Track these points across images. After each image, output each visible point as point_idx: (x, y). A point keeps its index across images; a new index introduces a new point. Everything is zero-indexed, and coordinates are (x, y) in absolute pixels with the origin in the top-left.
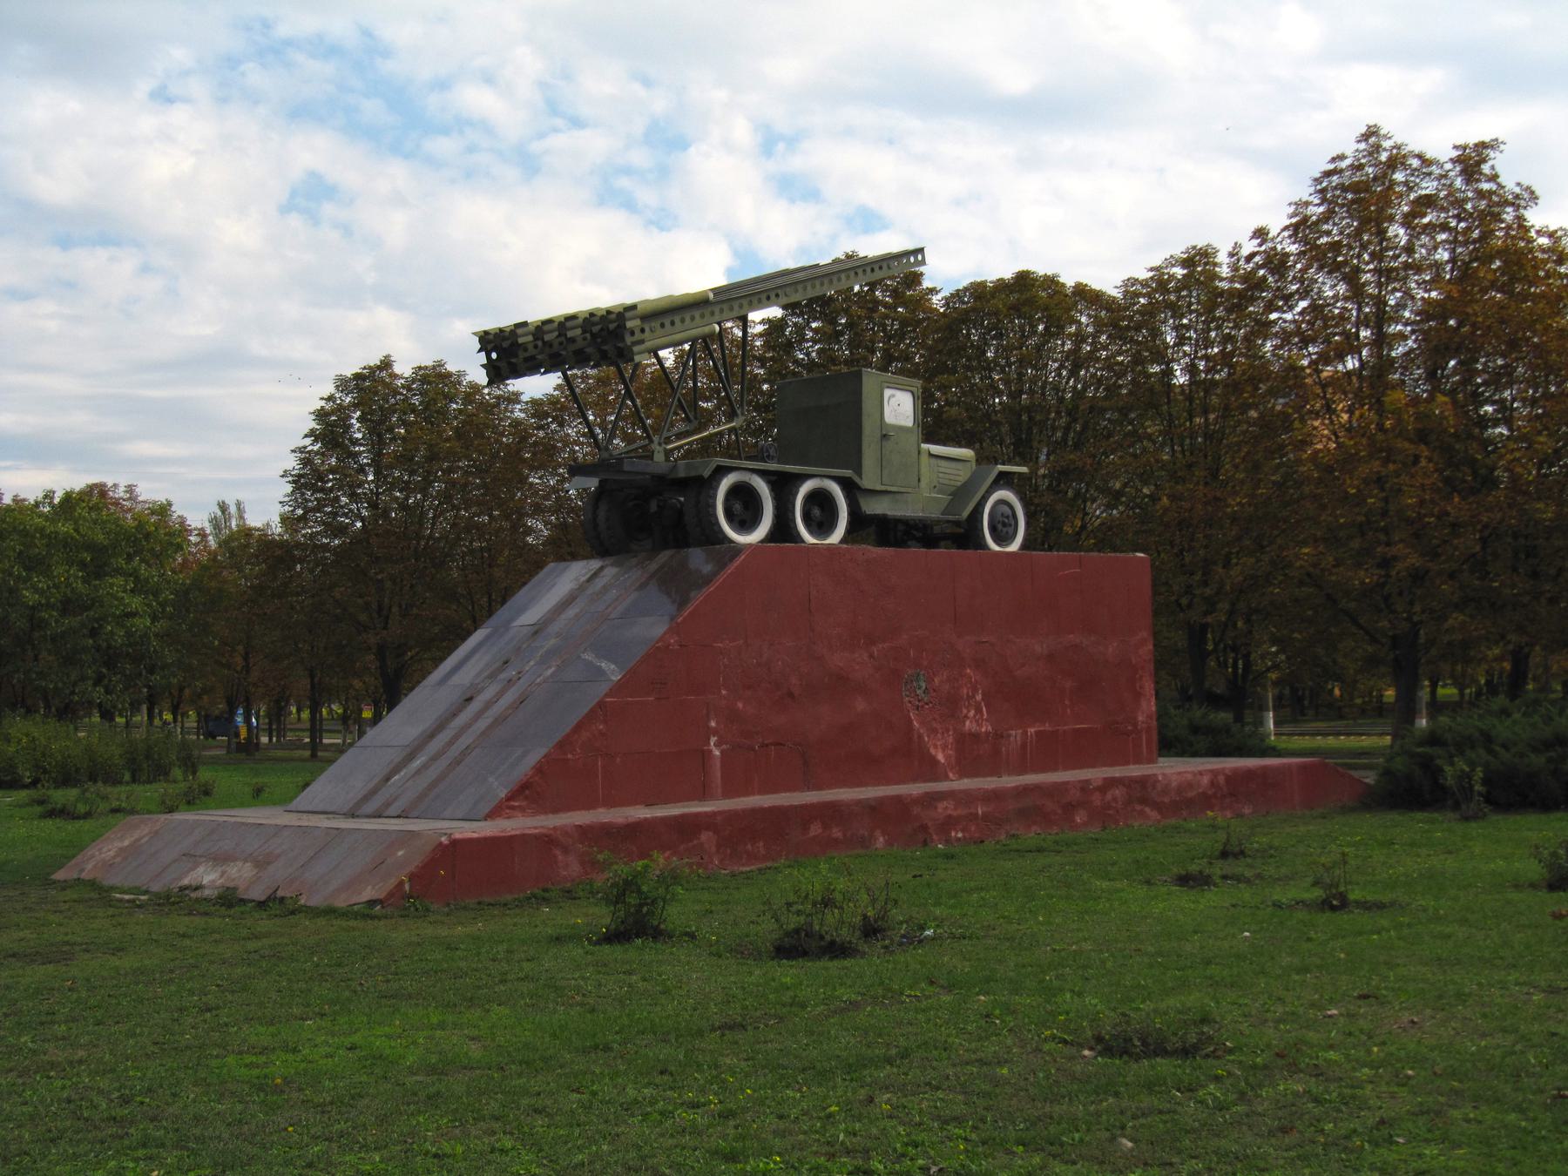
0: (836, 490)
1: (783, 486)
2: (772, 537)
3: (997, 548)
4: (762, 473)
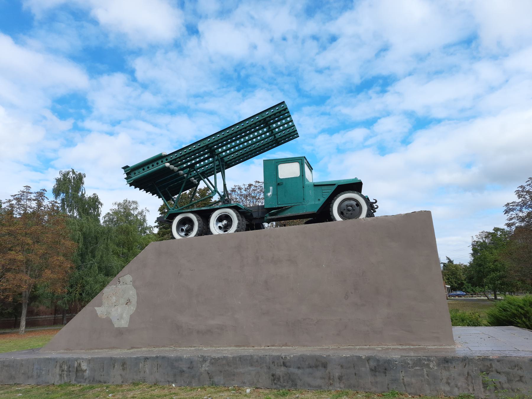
4: (192, 212)
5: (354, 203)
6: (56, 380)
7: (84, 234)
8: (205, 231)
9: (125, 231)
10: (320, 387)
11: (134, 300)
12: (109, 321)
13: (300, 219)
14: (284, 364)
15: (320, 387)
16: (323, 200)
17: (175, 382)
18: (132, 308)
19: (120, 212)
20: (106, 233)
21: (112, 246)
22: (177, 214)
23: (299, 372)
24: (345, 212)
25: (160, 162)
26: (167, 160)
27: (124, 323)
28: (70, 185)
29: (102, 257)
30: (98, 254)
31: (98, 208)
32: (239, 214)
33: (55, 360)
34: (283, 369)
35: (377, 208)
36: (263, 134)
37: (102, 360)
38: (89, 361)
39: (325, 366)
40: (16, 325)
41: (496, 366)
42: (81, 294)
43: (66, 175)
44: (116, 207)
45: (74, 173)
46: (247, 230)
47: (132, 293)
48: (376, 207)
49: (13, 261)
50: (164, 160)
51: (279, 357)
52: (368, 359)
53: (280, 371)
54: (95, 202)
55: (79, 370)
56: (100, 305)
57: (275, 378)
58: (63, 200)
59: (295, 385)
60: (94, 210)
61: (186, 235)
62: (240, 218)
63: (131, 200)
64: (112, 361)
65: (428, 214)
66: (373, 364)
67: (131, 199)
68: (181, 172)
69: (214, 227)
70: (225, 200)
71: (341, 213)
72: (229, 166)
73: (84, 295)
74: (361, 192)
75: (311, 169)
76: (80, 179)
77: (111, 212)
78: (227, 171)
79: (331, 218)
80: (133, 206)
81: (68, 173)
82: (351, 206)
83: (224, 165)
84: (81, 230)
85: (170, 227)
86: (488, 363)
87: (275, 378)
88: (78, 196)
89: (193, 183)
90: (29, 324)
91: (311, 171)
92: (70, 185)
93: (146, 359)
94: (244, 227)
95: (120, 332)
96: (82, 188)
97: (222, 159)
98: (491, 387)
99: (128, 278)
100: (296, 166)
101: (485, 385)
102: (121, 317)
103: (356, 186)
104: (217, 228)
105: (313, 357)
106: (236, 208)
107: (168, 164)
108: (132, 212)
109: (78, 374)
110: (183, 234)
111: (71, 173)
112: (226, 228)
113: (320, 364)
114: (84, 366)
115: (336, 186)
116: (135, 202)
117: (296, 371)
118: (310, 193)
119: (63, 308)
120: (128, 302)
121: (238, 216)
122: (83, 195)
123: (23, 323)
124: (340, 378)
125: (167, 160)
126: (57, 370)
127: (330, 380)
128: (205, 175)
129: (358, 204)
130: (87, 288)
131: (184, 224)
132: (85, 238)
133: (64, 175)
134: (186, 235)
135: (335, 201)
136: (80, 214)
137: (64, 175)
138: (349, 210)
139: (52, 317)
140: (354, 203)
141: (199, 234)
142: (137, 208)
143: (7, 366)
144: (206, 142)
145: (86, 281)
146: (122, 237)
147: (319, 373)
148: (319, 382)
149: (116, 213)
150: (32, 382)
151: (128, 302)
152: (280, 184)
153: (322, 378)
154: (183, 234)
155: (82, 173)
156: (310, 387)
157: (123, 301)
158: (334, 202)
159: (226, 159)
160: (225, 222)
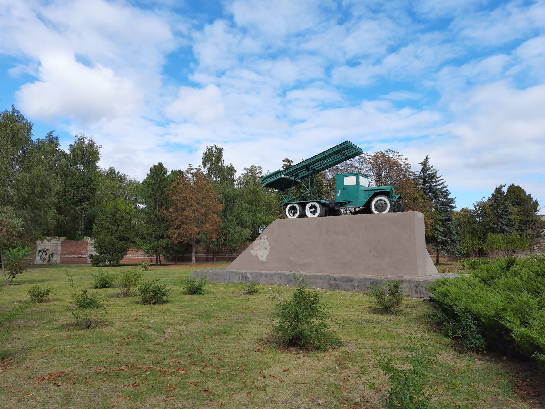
1: (303, 206)
4: (296, 203)
5: (383, 202)
6: (237, 281)
7: (225, 196)
8: (303, 215)
9: (253, 192)
10: (349, 289)
11: (268, 248)
12: (257, 258)
14: (335, 280)
15: (349, 289)
16: (368, 198)
17: (288, 284)
18: (268, 252)
19: (249, 175)
20: (239, 195)
21: (244, 204)
22: (288, 204)
23: (341, 283)
27: (264, 259)
29: (238, 213)
30: (236, 210)
31: (233, 174)
33: (236, 273)
34: (334, 281)
36: (339, 157)
37: (257, 273)
38: (251, 274)
39: (352, 281)
40: (190, 260)
41: (422, 284)
42: (225, 240)
43: (210, 150)
44: (245, 172)
45: (216, 147)
46: (326, 215)
47: (267, 244)
49: (187, 217)
51: (332, 277)
52: (370, 279)
53: (333, 282)
54: (231, 170)
55: (246, 277)
56: (252, 249)
57: (330, 285)
58: (209, 169)
59: (339, 288)
60: (231, 176)
61: (294, 215)
63: (256, 166)
64: (261, 275)
66: (372, 281)
67: (256, 165)
68: (291, 178)
69: (308, 212)
71: (376, 208)
73: (227, 241)
76: (219, 152)
77: (242, 176)
80: (258, 170)
81: (212, 148)
84: (223, 193)
85: (285, 208)
86: (418, 283)
87: (330, 285)
88: (219, 165)
90: (196, 260)
93: (276, 274)
94: (324, 212)
95: (263, 263)
96: (222, 159)
98: (419, 293)
99: (265, 237)
100: (354, 178)
101: (417, 292)
102: (262, 256)
104: (310, 214)
105: (347, 277)
107: (283, 176)
108: (258, 175)
110: (292, 215)
111: (214, 148)
112: (314, 213)
113: (351, 280)
114: (249, 276)
116: (260, 168)
117: (340, 283)
118: (362, 194)
119: (224, 250)
120: (266, 249)
122: (222, 165)
123: (193, 258)
124: (358, 286)
126: (237, 277)
127: (353, 287)
129: (385, 203)
130: (229, 235)
131: (292, 209)
132: (225, 198)
133: (209, 150)
134: (294, 215)
136: (221, 180)
137: (209, 150)
139: (205, 255)
140: (383, 202)
141: (300, 216)
142: (261, 172)
143: (215, 274)
145: (228, 231)
146: (251, 196)
147: (349, 284)
148: (349, 287)
149: (246, 176)
150: (226, 282)
151: (266, 249)
153: (350, 286)
154: (292, 215)
155: (221, 147)
156: (345, 289)
157: (263, 248)
160: (313, 209)
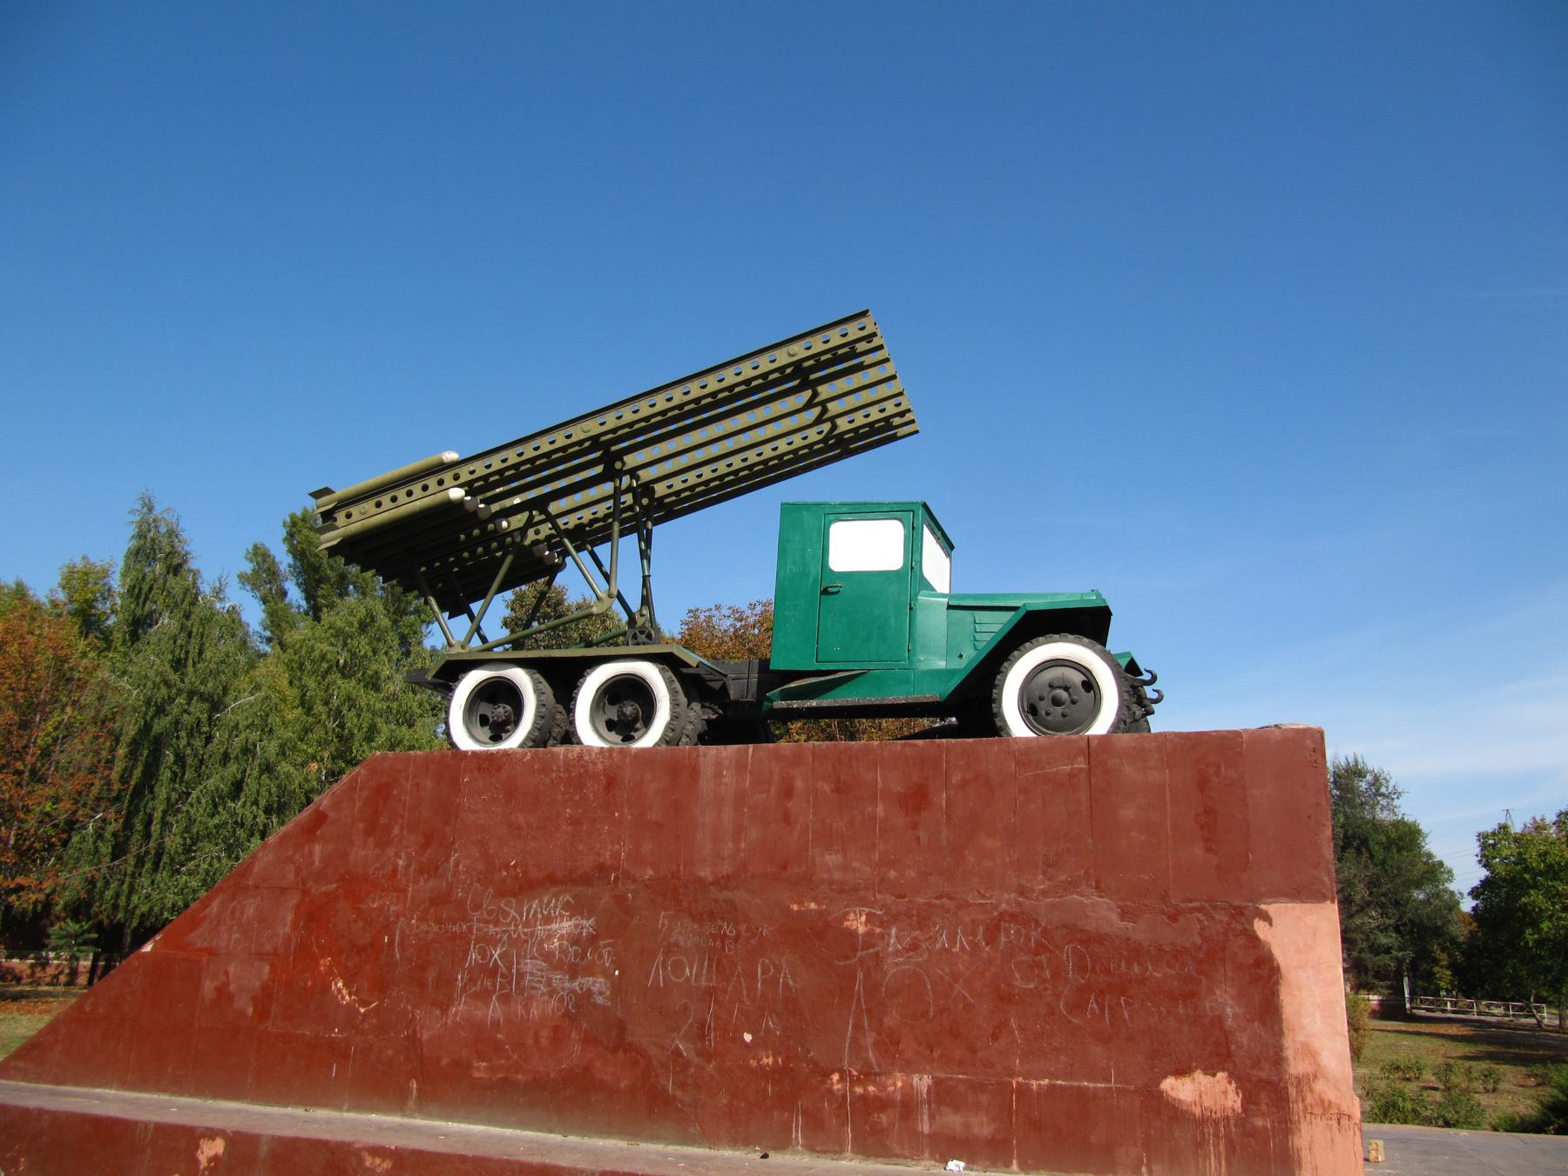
0: (651, 673)
1: (562, 679)
2: (539, 739)
3: (464, 741)
5: (1077, 678)
13: (866, 716)
16: (970, 657)
24: (1043, 707)
25: (432, 482)
26: (456, 477)
28: (158, 556)
32: (677, 685)
35: (1157, 701)
36: (784, 423)
48: (1155, 696)
50: (447, 477)
62: (683, 699)
65: (1321, 733)
70: (639, 633)
71: (1030, 710)
72: (670, 510)
74: (1104, 644)
75: (948, 545)
78: (660, 532)
79: (991, 725)
82: (1066, 689)
83: (648, 512)
89: (541, 559)
91: (948, 555)
92: (158, 556)
97: (647, 488)
103: (1090, 622)
106: (667, 661)
107: (456, 493)
109: (595, 638)
112: (626, 728)
115: (1021, 613)
121: (673, 692)
125: (456, 477)
128: (587, 537)
129: (1090, 685)
135: (1012, 665)
138: (1057, 702)
140: (1077, 678)
144: (592, 427)
152: (830, 587)
158: (1008, 670)
159: (660, 489)
